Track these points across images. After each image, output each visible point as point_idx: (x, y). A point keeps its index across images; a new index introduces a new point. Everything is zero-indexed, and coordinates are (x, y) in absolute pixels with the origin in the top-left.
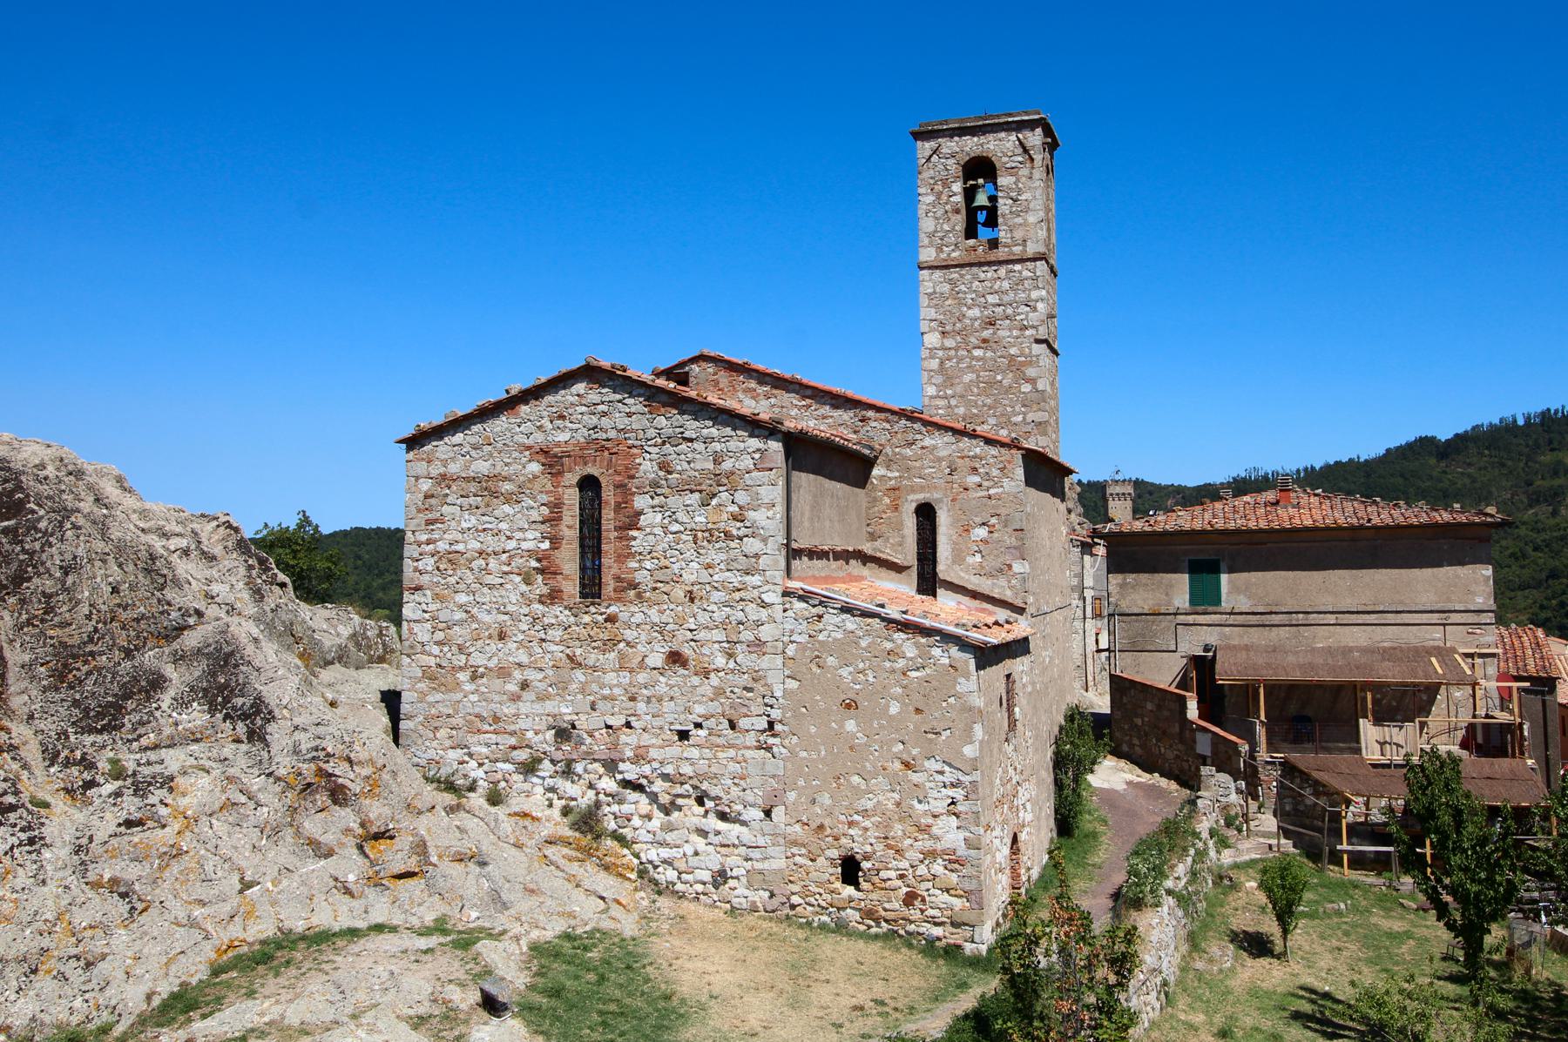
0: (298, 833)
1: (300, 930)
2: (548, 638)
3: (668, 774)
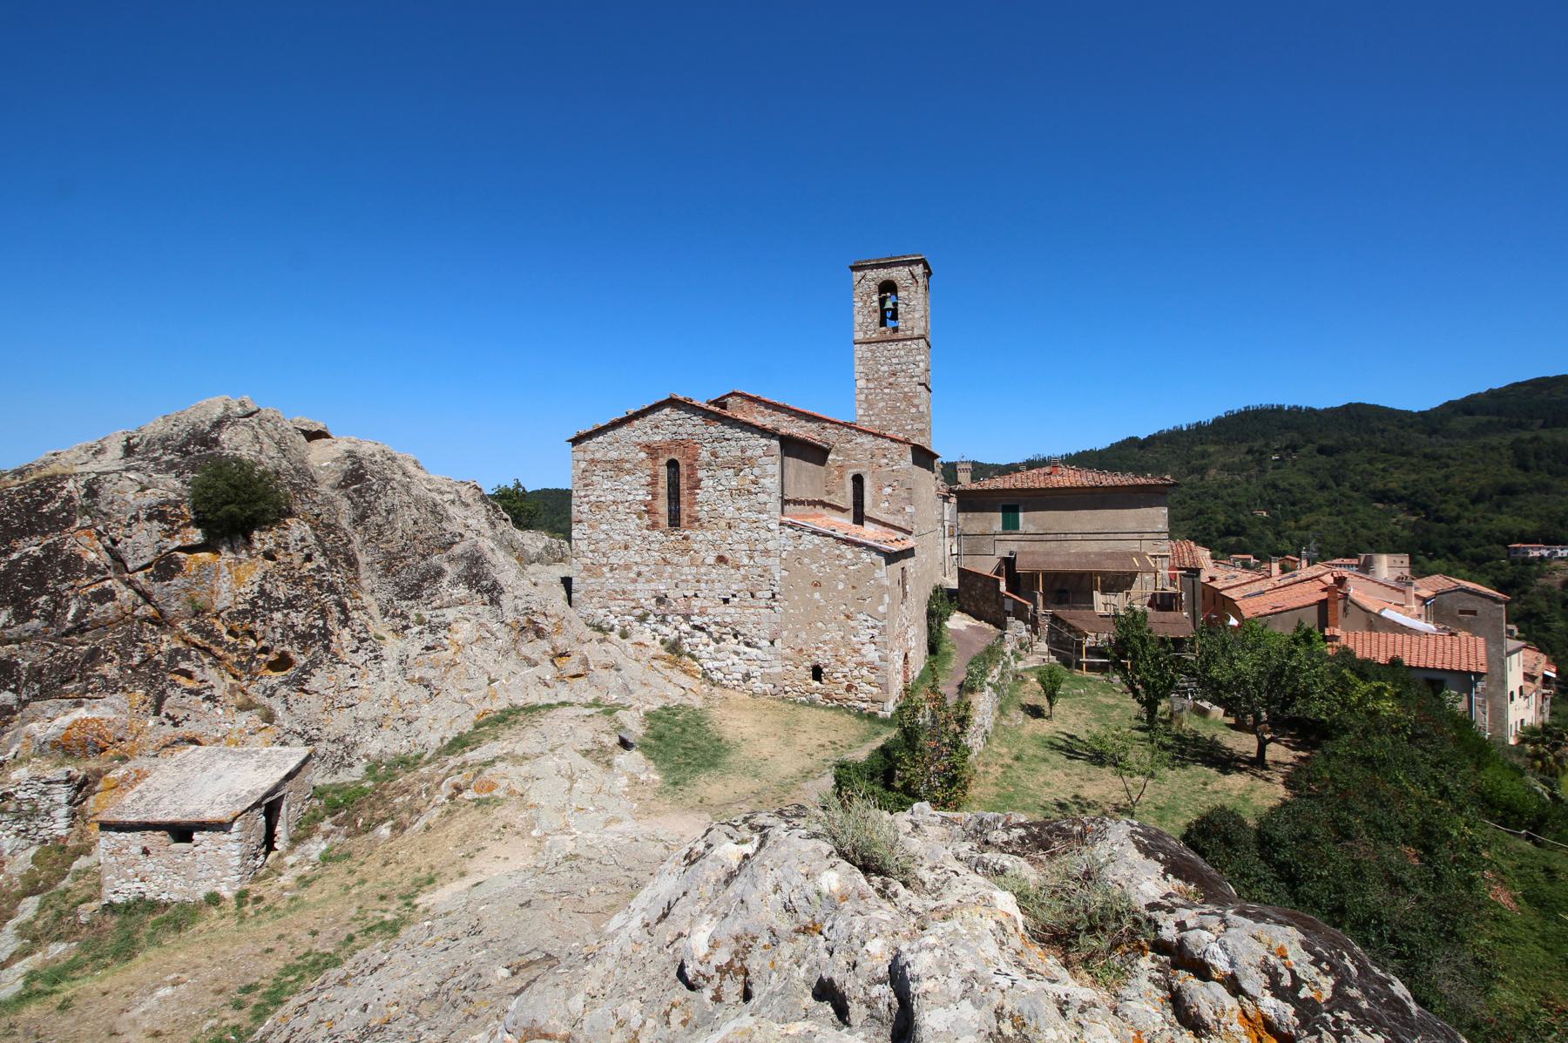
0: (518, 654)
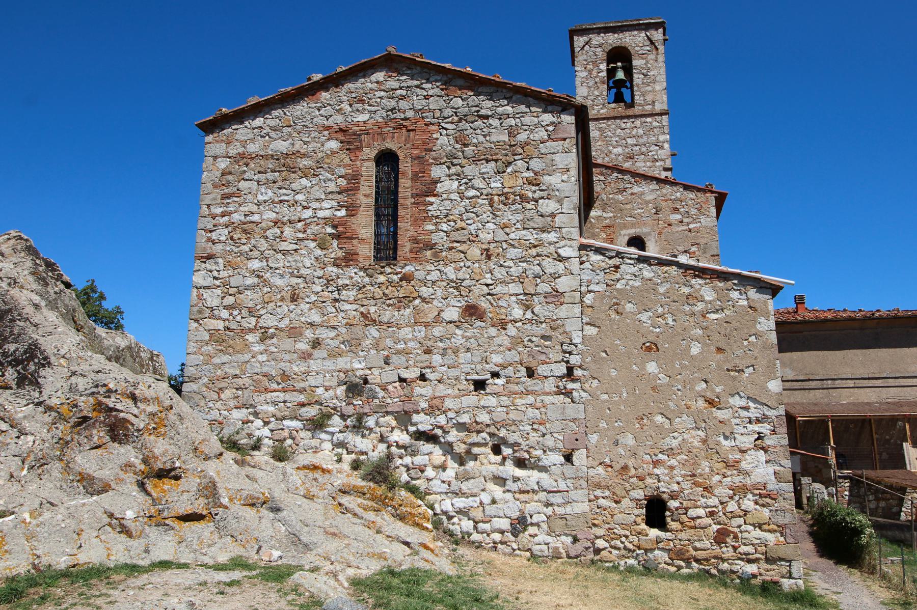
0: (67, 469)
1: (63, 566)
2: (342, 298)
3: (465, 423)
